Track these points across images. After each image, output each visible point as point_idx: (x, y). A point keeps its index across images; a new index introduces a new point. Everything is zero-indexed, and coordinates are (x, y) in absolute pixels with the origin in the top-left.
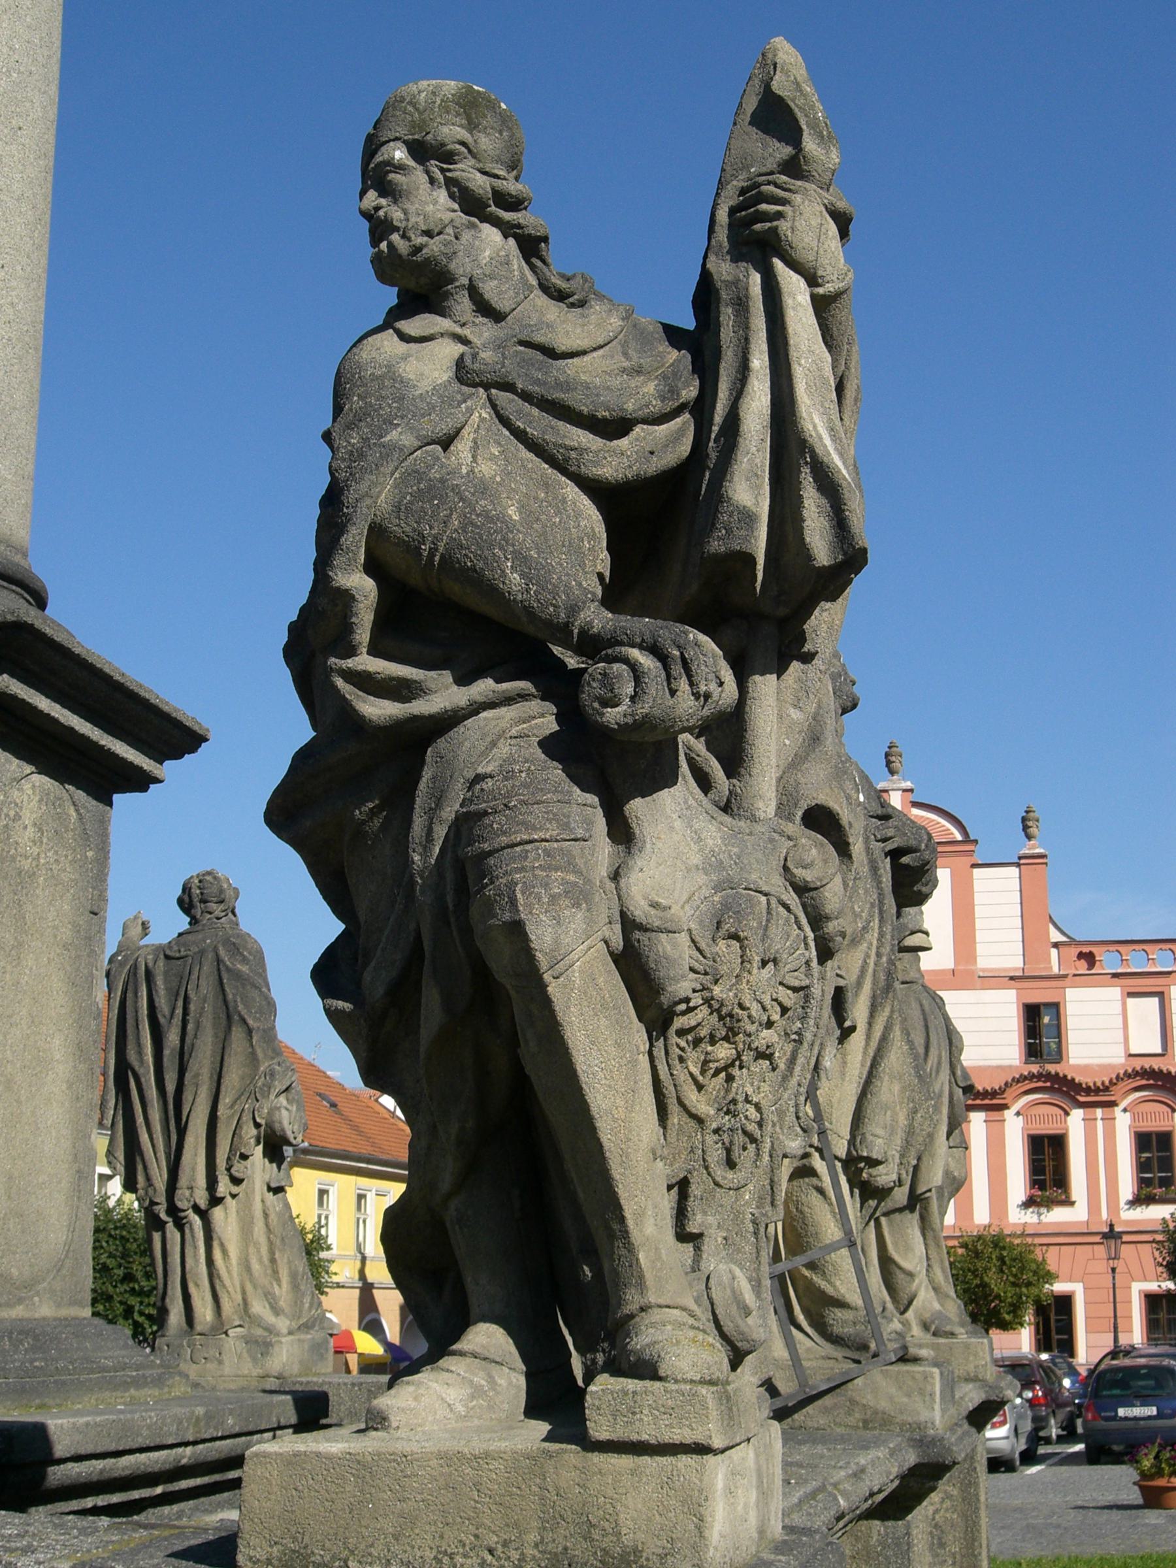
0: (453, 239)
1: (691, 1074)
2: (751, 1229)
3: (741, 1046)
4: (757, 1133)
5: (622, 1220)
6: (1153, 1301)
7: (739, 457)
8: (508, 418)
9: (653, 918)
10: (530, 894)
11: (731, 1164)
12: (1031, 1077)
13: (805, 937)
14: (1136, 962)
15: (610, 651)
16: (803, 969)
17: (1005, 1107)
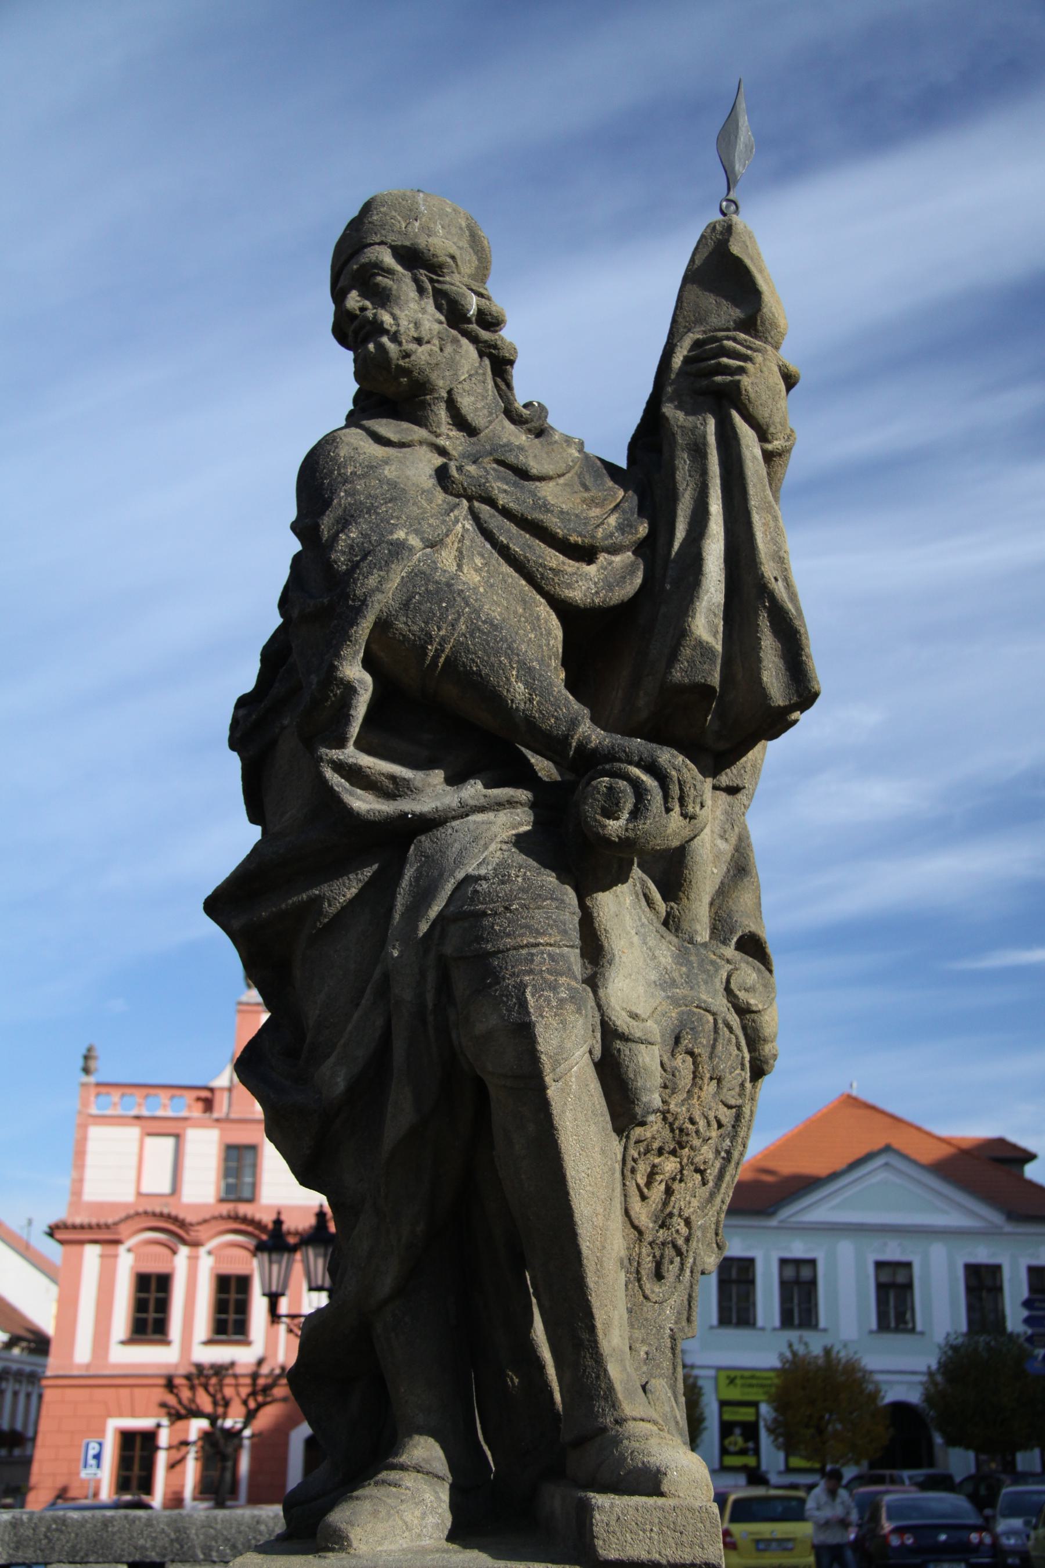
0: (438, 350)
1: (638, 1186)
2: (669, 1345)
3: (685, 1160)
4: (684, 1248)
5: (592, 1329)
7: (702, 595)
8: (491, 532)
9: (636, 1029)
10: (540, 997)
11: (659, 1276)
13: (743, 1058)
14: (164, 1107)
15: (607, 767)
16: (737, 1089)
17: (117, 1242)
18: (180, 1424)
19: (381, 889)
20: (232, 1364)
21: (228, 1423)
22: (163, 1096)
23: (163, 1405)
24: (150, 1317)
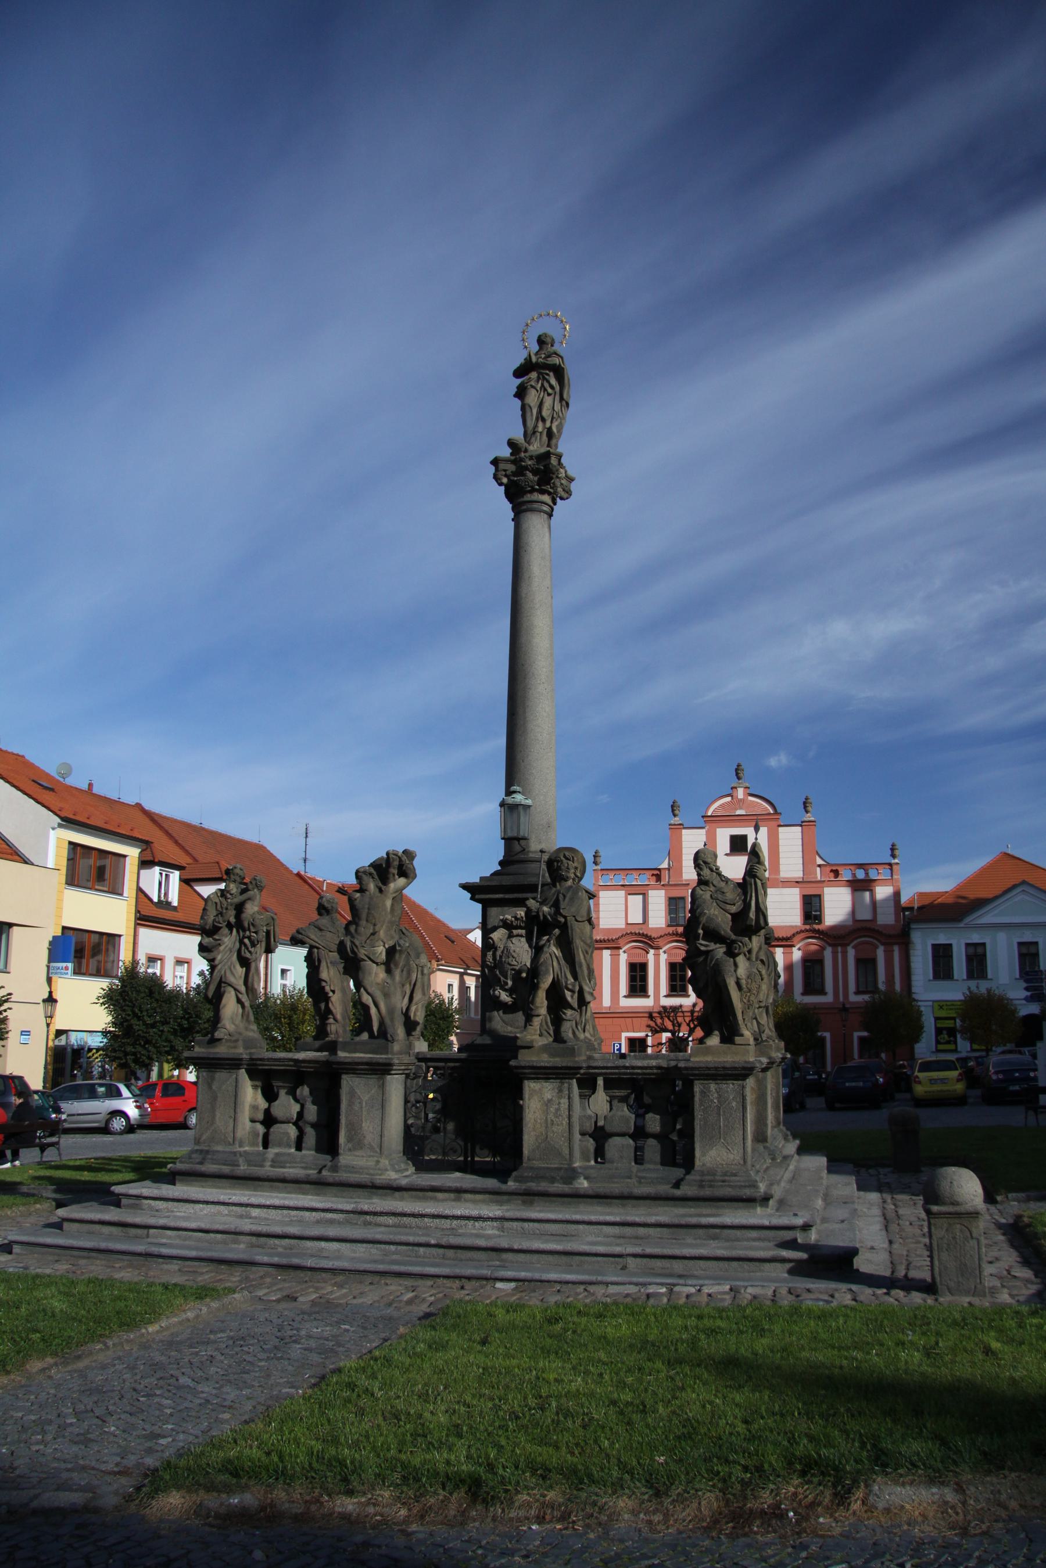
6: (861, 1039)
12: (807, 931)
14: (633, 879)
17: (619, 948)
18: (657, 1035)
19: (706, 960)
20: (681, 1006)
21: (681, 1034)
22: (635, 874)
23: (648, 1026)
24: (638, 984)
